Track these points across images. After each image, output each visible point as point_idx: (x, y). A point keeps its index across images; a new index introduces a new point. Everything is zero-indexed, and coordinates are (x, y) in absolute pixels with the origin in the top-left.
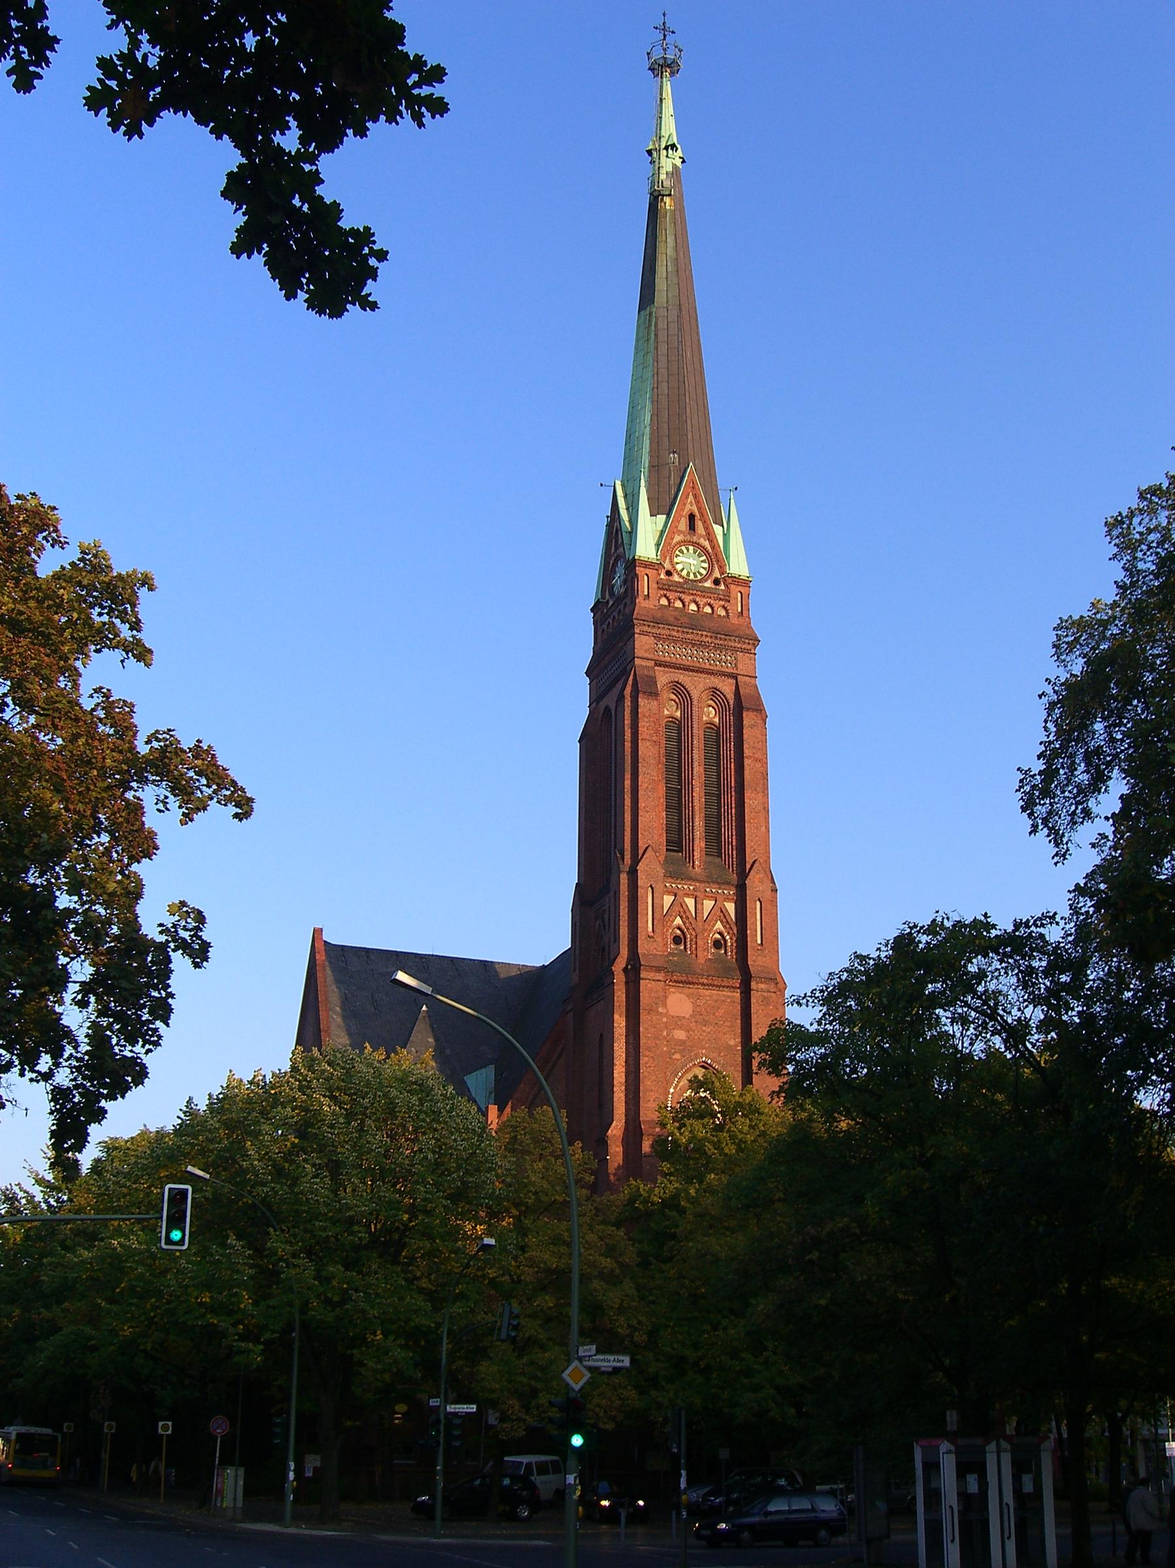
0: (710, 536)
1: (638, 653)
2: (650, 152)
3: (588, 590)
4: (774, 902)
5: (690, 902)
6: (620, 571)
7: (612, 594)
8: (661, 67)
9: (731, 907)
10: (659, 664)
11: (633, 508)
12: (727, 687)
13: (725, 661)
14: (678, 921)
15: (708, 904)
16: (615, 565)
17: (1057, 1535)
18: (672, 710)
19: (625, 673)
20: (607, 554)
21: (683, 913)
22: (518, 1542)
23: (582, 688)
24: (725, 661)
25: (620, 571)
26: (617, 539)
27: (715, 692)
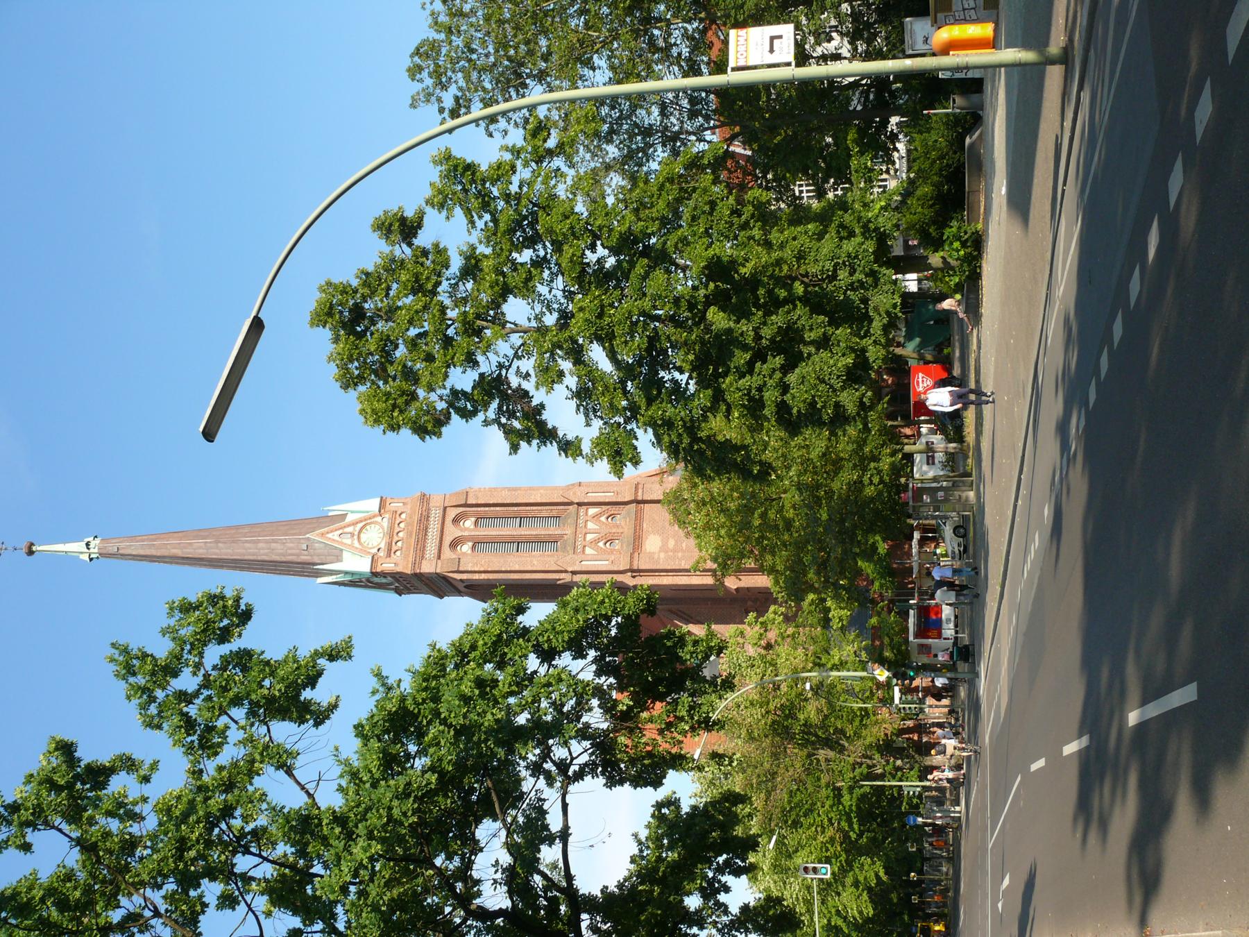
0: (354, 524)
1: (432, 570)
2: (91, 559)
3: (391, 596)
4: (588, 485)
5: (589, 537)
6: (376, 580)
7: (391, 584)
8: (31, 553)
9: (592, 511)
10: (439, 557)
11: (331, 572)
12: (452, 513)
13: (435, 515)
14: (601, 544)
15: (590, 525)
16: (1110, 686)
17: (1007, 47)
18: (466, 548)
19: (445, 578)
20: (366, 587)
21: (596, 541)
22: (1121, 59)
23: (448, 600)
24: (435, 515)
25: (376, 580)
26: (356, 582)
27: (456, 521)
